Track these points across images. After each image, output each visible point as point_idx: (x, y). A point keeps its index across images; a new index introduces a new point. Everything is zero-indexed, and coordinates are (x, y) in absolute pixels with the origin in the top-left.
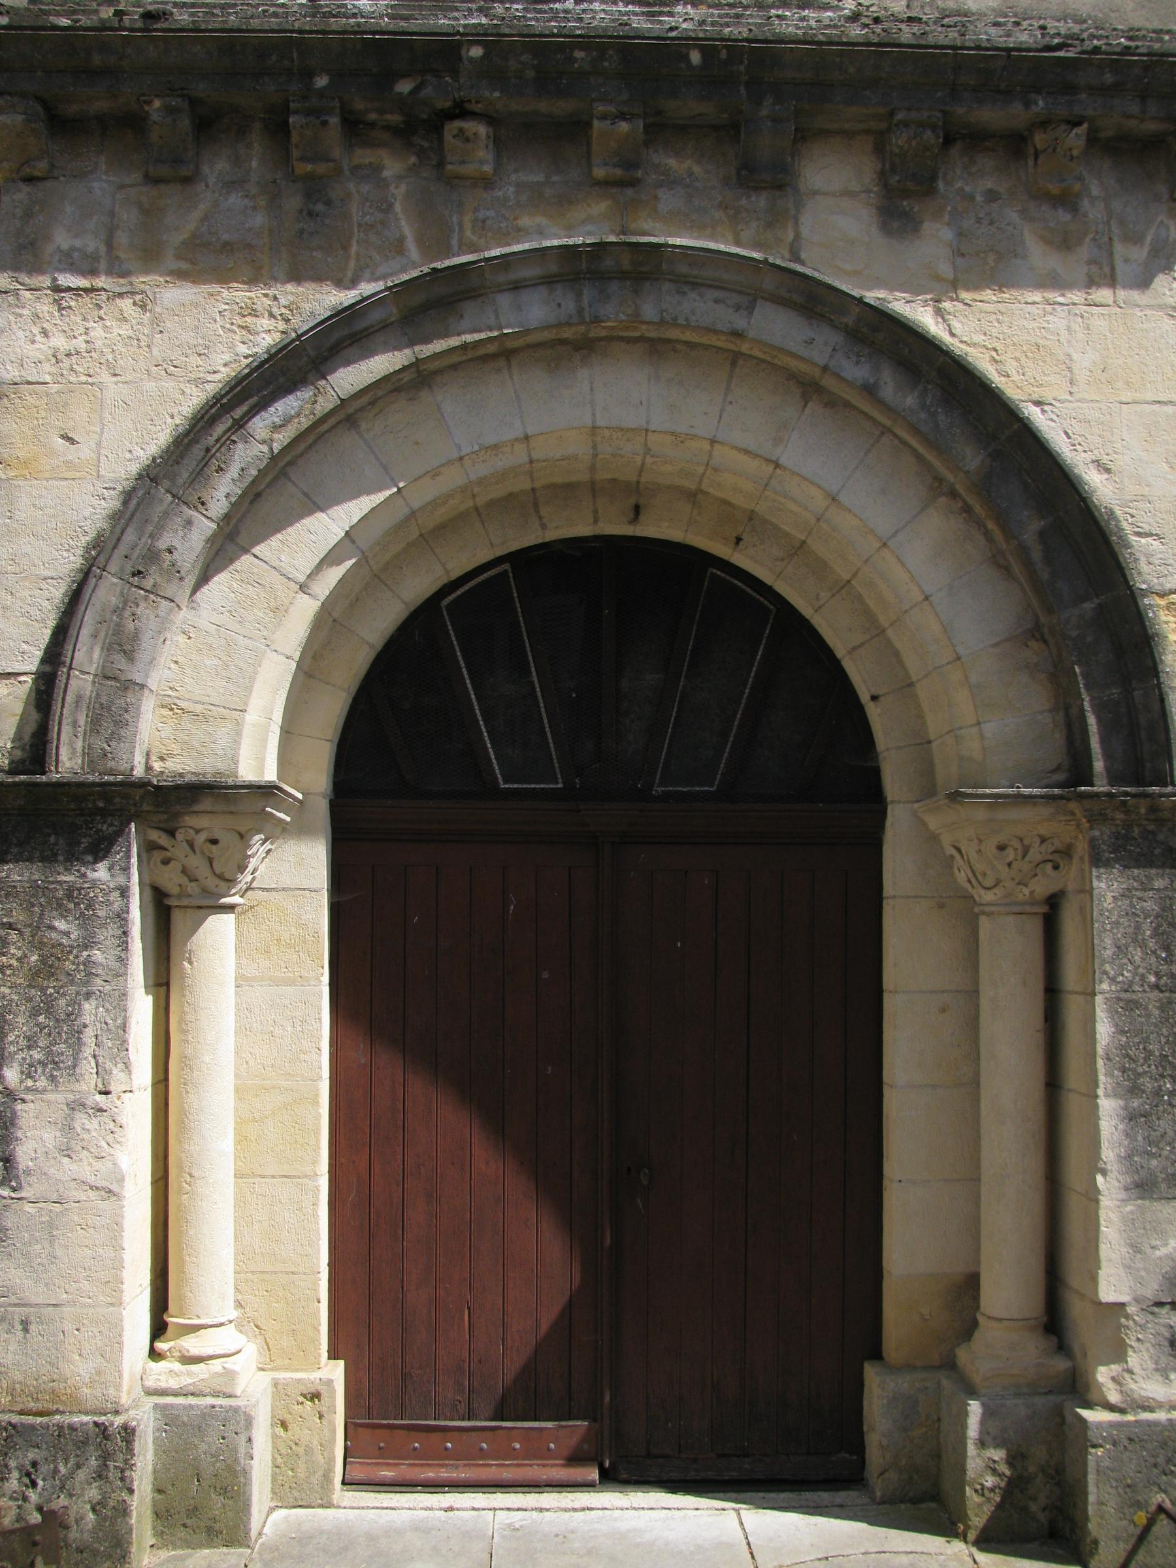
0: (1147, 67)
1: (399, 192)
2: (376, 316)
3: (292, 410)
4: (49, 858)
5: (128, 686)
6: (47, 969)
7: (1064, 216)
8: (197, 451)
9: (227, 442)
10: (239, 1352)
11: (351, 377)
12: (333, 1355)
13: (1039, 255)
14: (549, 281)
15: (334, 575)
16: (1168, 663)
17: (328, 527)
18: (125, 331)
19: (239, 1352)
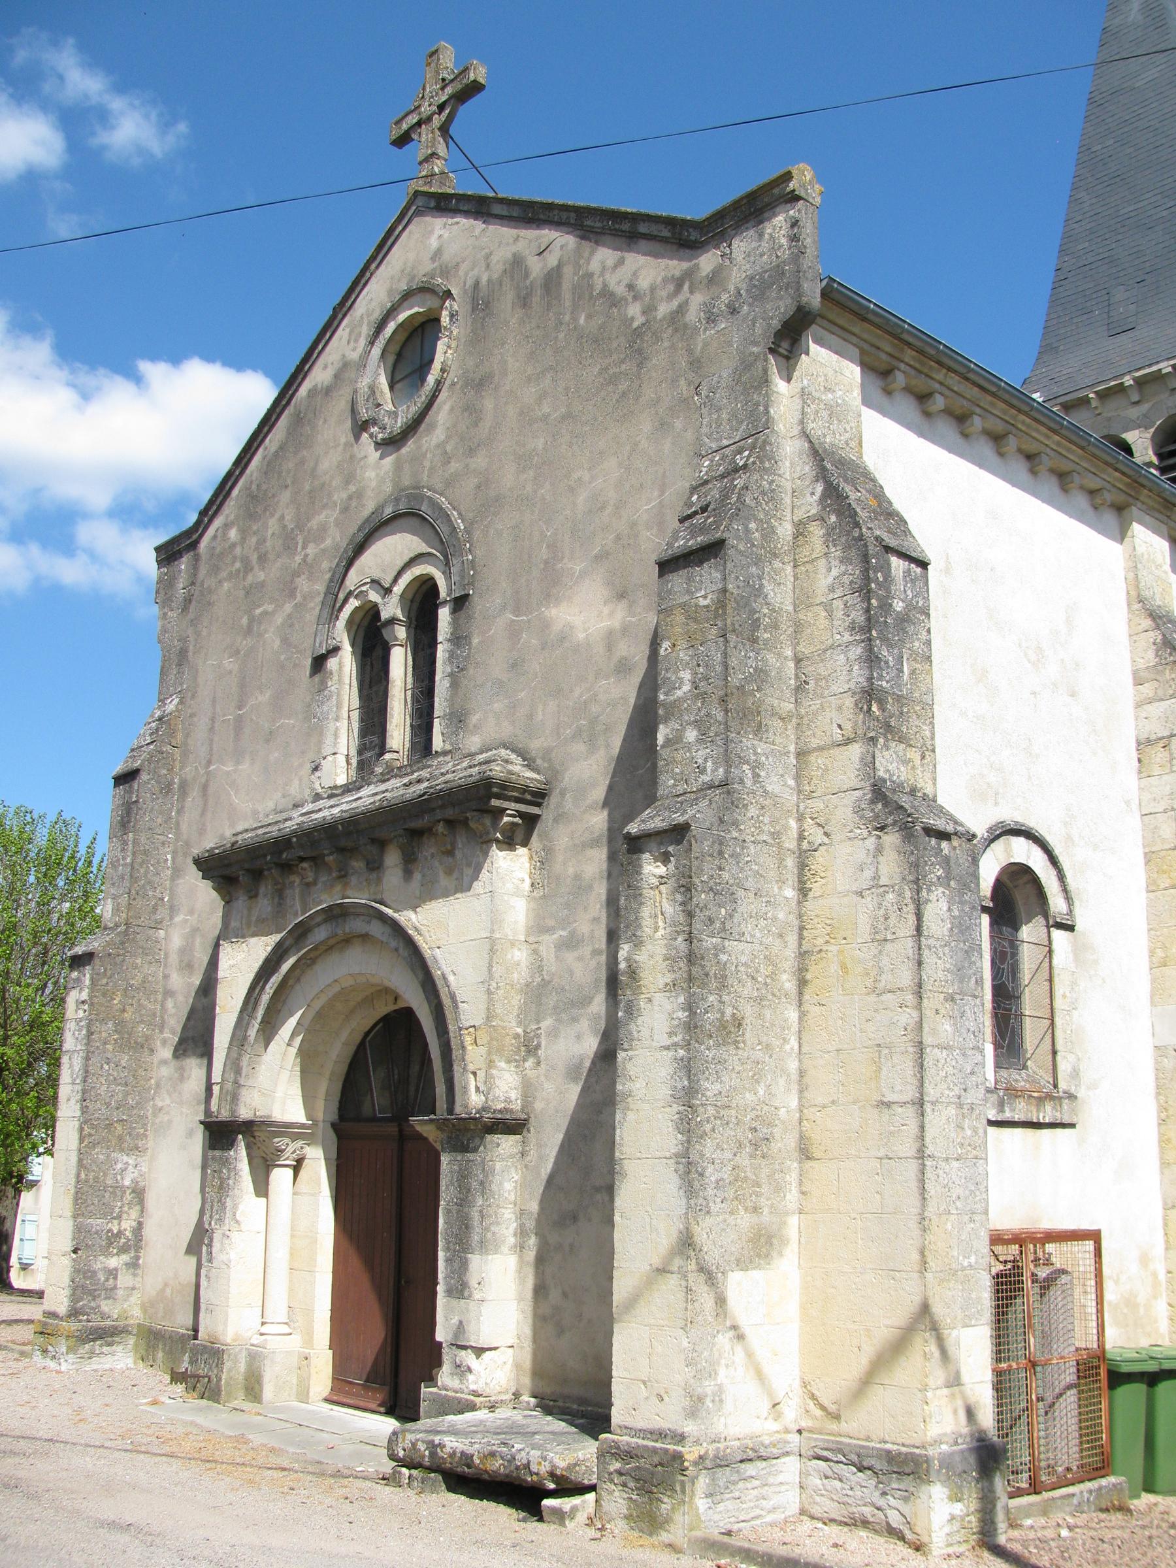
0: (449, 794)
1: (297, 891)
2: (288, 943)
3: (275, 980)
4: (223, 1149)
5: (240, 1086)
6: (221, 1187)
7: (450, 859)
8: (252, 1000)
9: (260, 994)
10: (495, 1349)
11: (285, 967)
12: (440, 1344)
13: (444, 881)
14: (325, 921)
15: (299, 1039)
16: (639, 1023)
17: (292, 1022)
18: (691, 735)
19: (495, 1349)
